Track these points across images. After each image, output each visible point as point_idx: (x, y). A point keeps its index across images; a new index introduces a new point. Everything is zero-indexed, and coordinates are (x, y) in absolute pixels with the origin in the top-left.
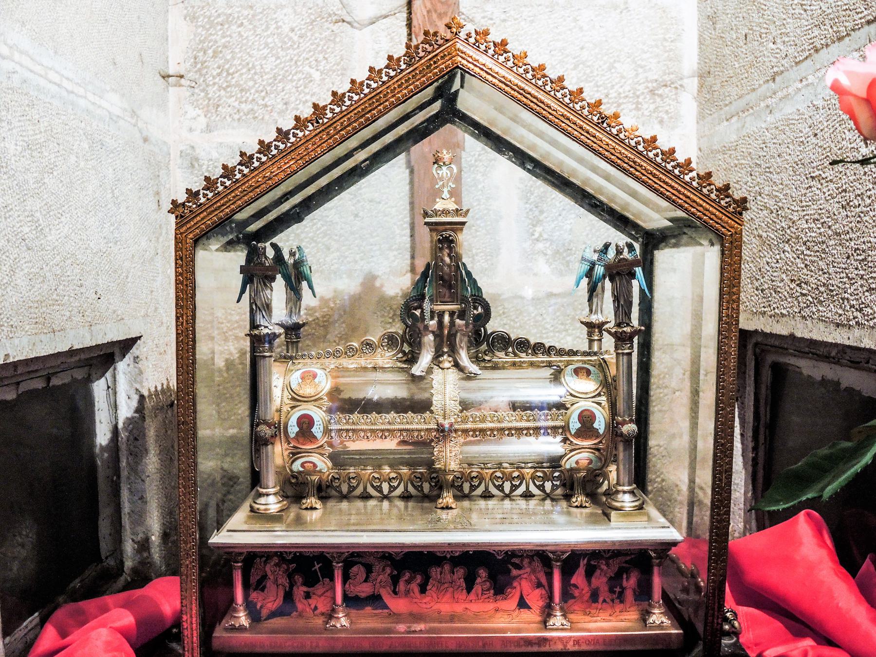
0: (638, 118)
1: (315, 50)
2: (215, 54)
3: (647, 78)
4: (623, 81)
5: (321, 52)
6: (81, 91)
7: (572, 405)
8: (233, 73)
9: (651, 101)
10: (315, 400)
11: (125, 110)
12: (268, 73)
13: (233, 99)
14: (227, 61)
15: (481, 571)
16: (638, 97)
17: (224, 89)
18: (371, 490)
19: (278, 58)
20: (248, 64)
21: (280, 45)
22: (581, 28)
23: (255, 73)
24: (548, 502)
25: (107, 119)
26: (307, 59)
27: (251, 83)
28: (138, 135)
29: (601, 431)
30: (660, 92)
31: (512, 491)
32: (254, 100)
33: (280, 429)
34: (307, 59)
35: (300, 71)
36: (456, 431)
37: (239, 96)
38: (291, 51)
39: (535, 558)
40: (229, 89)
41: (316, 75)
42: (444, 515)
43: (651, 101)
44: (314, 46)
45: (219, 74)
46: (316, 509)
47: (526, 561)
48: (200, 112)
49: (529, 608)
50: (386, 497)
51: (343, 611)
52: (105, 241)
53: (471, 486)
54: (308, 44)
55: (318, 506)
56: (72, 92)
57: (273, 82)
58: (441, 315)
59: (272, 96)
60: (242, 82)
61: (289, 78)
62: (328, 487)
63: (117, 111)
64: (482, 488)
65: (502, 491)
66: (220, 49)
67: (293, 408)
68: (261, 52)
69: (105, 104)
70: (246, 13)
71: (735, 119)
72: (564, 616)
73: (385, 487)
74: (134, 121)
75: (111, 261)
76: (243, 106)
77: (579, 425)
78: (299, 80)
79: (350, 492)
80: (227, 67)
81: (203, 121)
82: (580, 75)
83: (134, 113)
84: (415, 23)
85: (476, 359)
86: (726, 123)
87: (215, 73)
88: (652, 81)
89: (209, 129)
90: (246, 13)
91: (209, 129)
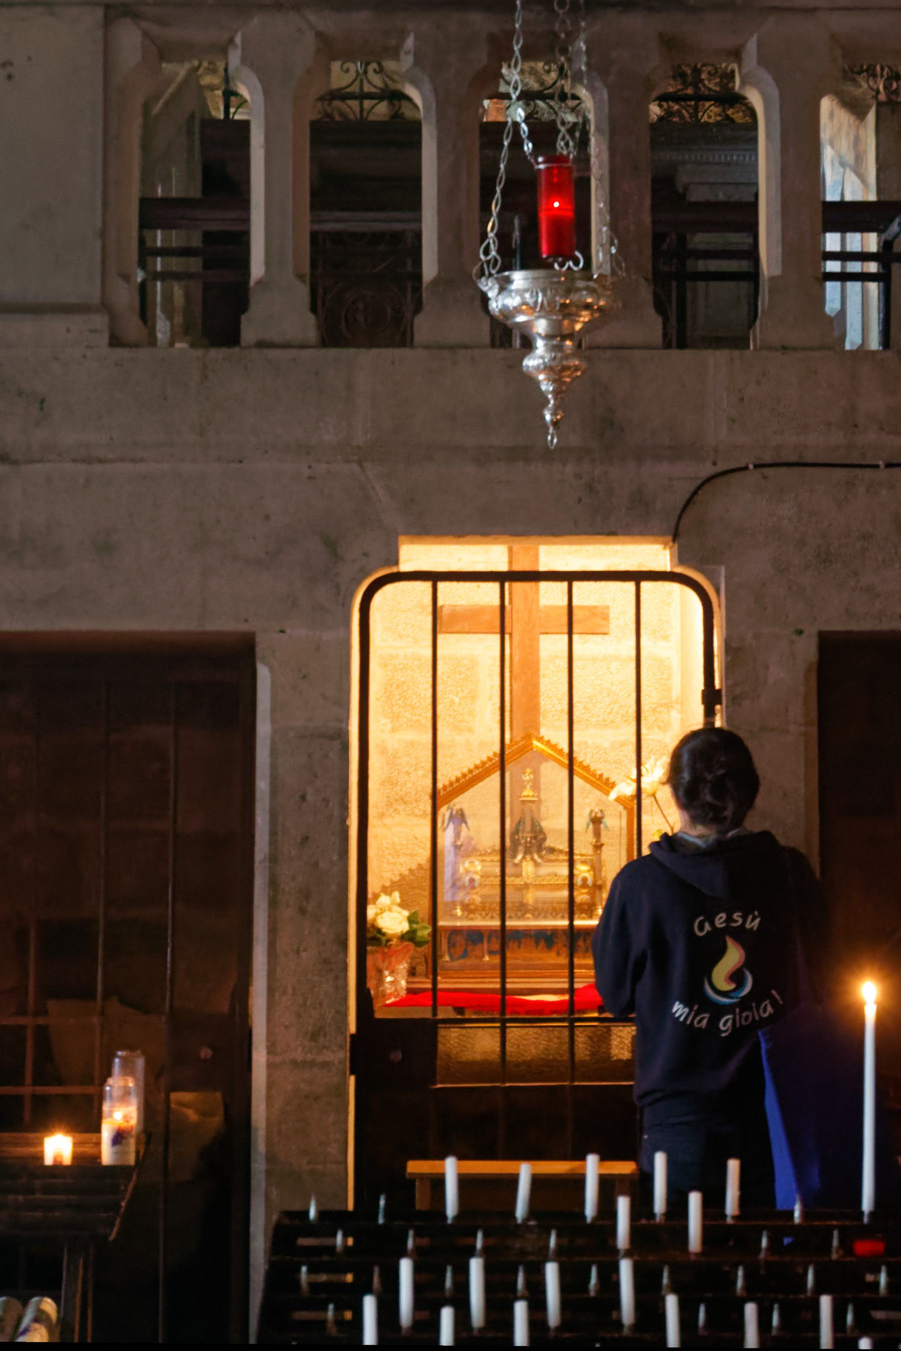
2: (398, 687)
22: (611, 673)
30: (659, 709)
41: (457, 700)
70: (416, 663)
84: (514, 671)
85: (541, 857)
90: (416, 663)
91: (394, 730)
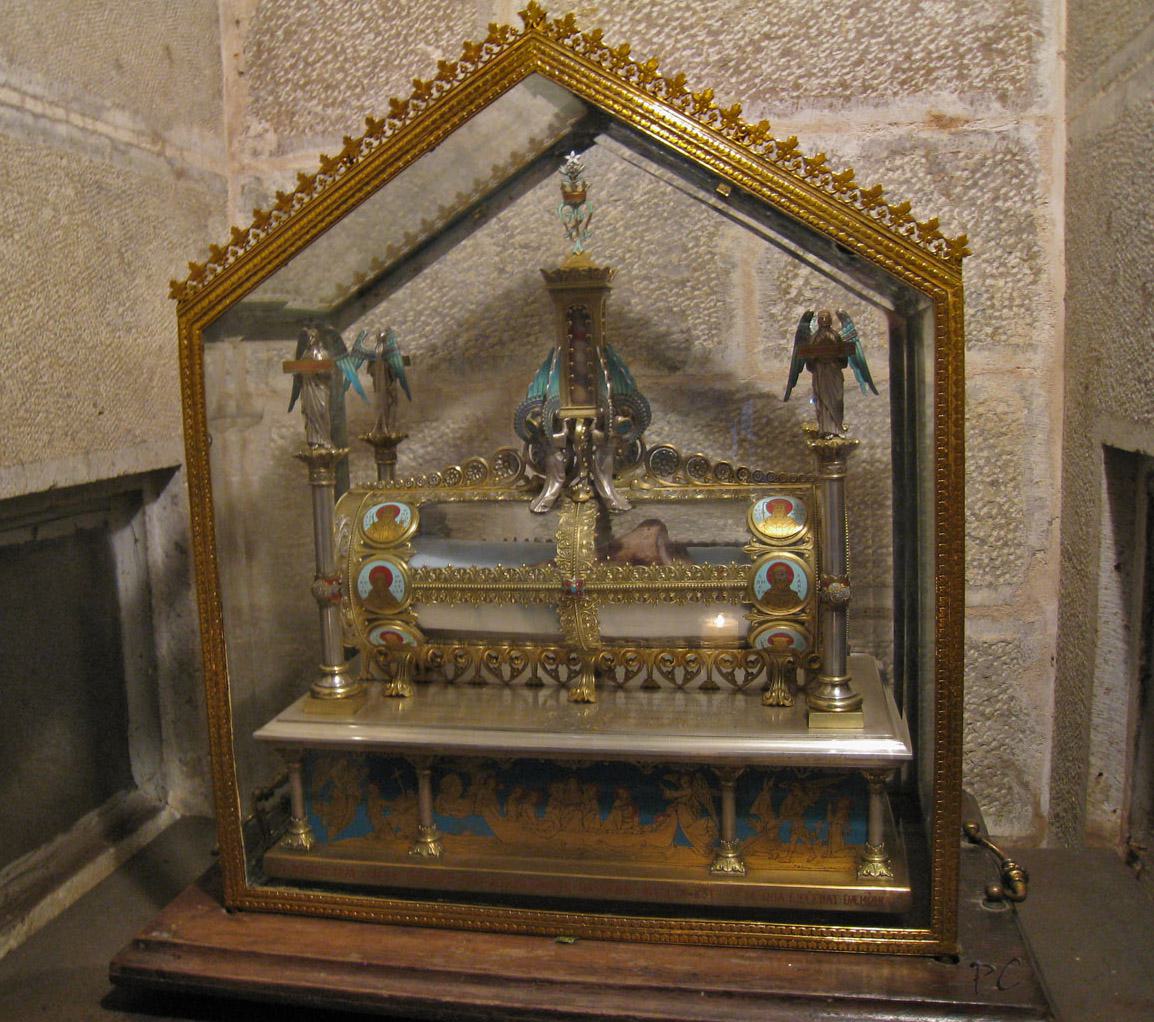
0: (962, 92)
1: (434, 15)
2: (288, 34)
3: (977, 22)
4: (936, 30)
5: (441, 19)
6: (60, 113)
7: (760, 556)
8: (315, 62)
9: (985, 62)
10: (396, 548)
11: (140, 133)
12: (365, 57)
13: (315, 102)
14: (305, 45)
15: (621, 791)
16: (962, 57)
17: (303, 87)
18: (717, 679)
19: (378, 34)
20: (334, 47)
21: (381, 13)
23: (346, 60)
24: (740, 697)
25: (109, 150)
26: (423, 31)
27: (340, 76)
28: (165, 168)
29: (802, 596)
31: (457, 675)
32: (344, 101)
33: (343, 587)
34: (423, 31)
35: (412, 51)
36: (589, 592)
37: (323, 96)
38: (396, 22)
39: (698, 775)
40: (308, 88)
42: (772, 713)
43: (985, 62)
44: (432, 11)
45: (293, 66)
46: (403, 696)
47: (684, 780)
48: (267, 125)
49: (690, 845)
50: (507, 685)
51: (433, 834)
52: (110, 328)
53: (687, 672)
54: (423, 8)
55: (407, 694)
56: (43, 116)
57: (372, 72)
58: (572, 423)
59: (372, 92)
60: (327, 76)
61: (396, 63)
62: (428, 669)
63: (124, 136)
64: (643, 675)
65: (673, 680)
66: (294, 28)
67: (364, 558)
68: (354, 27)
69: (101, 127)
71: (1113, 86)
72: (740, 858)
73: (506, 670)
74: (157, 148)
75: (120, 358)
76: (329, 111)
77: (767, 586)
78: (411, 65)
79: (457, 675)
80: (304, 53)
81: (271, 137)
82: (862, 25)
83: (157, 137)
86: (1101, 94)
87: (287, 65)
88: (986, 29)
89: (280, 150)
